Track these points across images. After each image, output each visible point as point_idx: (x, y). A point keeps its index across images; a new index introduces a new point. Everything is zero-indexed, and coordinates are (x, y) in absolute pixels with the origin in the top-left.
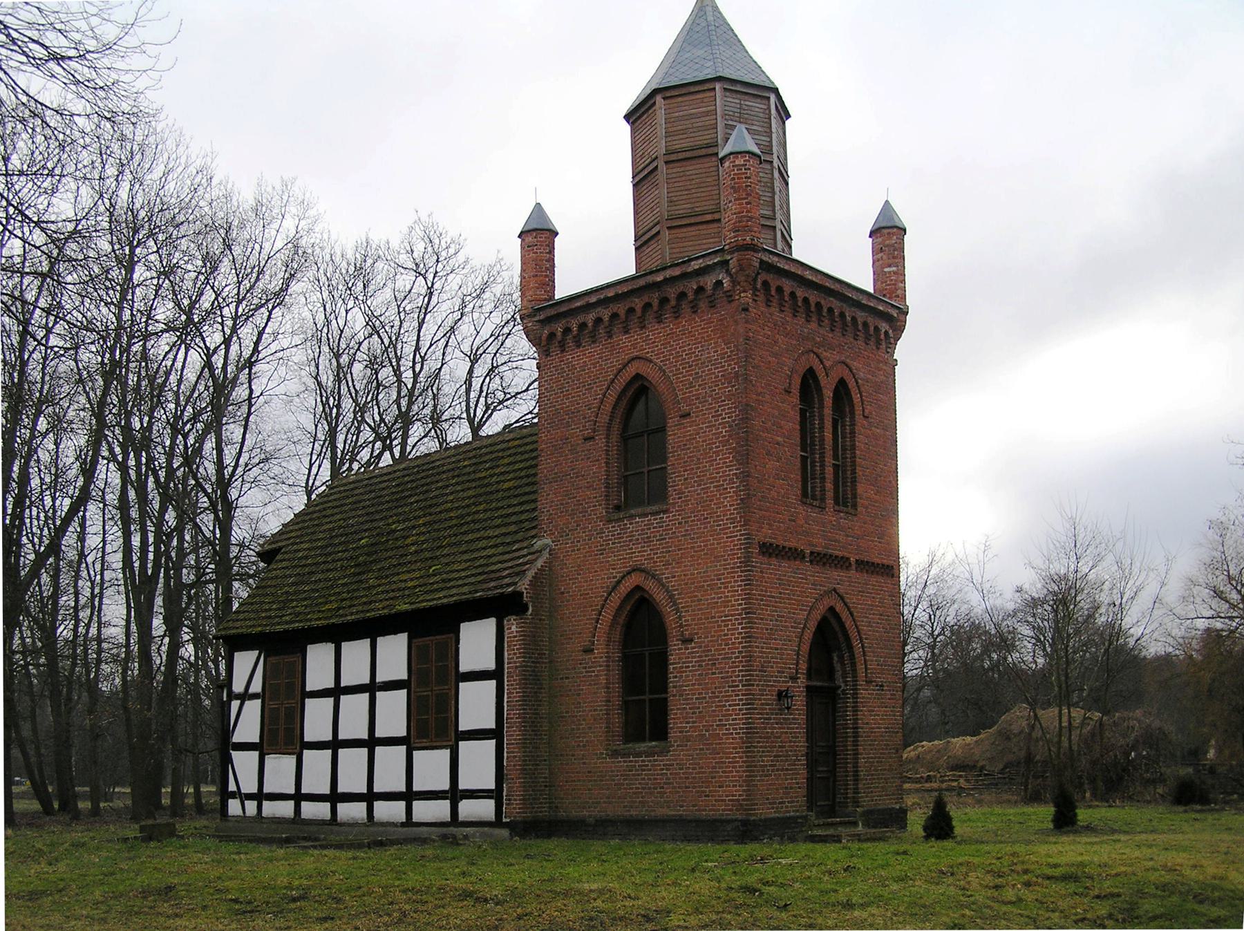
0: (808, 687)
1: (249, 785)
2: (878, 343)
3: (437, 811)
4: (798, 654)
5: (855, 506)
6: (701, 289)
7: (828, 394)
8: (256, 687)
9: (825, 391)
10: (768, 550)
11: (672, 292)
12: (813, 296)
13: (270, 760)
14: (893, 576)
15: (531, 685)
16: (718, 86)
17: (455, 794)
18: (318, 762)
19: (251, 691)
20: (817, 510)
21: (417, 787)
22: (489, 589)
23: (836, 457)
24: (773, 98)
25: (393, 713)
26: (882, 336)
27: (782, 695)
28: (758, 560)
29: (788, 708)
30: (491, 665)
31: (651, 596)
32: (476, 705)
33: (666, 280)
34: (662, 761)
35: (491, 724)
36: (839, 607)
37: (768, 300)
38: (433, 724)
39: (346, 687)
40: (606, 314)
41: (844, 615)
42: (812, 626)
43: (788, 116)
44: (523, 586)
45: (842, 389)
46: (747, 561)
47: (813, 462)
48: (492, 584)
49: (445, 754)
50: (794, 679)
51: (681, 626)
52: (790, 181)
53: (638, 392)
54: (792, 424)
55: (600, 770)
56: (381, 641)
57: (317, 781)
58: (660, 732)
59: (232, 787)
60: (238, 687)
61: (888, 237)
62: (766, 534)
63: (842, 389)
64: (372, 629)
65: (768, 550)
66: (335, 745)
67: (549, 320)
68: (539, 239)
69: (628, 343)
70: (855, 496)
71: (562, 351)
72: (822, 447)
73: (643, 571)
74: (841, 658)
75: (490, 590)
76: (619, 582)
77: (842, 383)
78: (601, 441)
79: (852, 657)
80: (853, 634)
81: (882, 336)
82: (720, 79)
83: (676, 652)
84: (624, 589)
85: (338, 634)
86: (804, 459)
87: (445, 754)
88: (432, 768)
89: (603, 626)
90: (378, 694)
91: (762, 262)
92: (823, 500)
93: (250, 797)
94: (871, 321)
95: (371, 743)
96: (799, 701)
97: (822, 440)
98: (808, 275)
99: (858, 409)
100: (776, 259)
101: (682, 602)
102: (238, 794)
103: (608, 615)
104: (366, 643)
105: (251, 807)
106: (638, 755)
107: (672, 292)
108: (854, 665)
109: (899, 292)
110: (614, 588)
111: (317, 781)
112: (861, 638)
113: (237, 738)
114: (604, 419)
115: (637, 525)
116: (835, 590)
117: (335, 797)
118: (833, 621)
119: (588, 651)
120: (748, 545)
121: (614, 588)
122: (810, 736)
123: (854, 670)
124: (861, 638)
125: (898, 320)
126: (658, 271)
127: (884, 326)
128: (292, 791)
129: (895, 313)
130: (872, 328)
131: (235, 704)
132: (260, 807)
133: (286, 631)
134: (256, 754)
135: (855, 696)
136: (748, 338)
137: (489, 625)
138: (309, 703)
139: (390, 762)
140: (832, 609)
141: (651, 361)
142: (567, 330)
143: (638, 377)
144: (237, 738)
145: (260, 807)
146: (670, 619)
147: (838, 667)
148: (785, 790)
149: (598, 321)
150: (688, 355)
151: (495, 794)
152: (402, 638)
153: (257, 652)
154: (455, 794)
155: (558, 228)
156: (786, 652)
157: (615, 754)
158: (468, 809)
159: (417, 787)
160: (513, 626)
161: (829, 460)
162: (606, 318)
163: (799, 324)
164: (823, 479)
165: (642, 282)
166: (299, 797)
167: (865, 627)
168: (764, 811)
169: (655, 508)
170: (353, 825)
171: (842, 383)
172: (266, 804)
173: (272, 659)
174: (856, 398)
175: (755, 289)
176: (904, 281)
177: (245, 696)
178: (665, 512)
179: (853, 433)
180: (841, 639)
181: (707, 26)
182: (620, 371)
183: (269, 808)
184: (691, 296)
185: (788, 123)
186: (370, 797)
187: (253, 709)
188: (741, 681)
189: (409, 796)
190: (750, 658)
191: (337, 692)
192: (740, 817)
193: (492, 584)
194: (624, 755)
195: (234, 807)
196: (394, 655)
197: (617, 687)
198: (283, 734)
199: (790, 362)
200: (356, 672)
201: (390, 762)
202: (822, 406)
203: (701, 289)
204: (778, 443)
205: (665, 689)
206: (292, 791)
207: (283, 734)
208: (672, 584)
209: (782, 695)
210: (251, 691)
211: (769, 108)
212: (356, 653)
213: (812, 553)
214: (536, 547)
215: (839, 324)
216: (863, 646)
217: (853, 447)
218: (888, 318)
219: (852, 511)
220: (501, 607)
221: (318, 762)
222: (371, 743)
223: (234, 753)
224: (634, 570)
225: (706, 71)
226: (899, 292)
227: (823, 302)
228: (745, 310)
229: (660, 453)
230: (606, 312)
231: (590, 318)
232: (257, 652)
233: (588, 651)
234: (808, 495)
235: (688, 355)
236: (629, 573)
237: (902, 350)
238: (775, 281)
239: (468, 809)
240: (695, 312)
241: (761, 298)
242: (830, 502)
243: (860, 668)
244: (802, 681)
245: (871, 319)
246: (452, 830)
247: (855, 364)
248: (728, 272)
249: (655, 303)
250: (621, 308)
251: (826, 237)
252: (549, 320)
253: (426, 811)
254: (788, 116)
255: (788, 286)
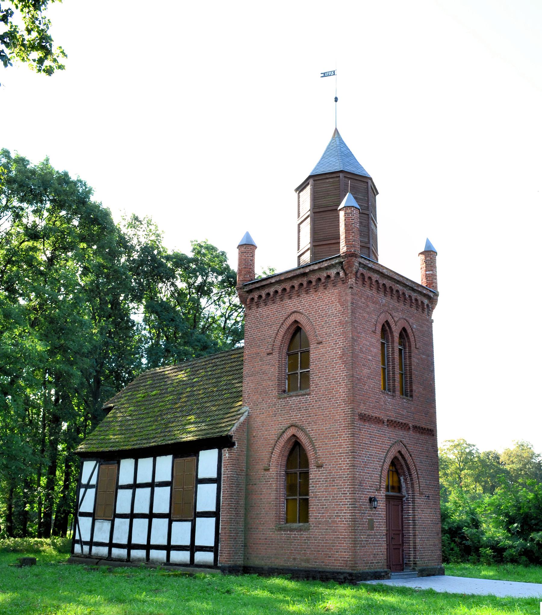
0: (386, 496)
1: (86, 537)
2: (423, 309)
3: (183, 557)
4: (381, 477)
5: (411, 396)
6: (328, 277)
7: (396, 335)
8: (93, 481)
9: (395, 334)
10: (364, 418)
11: (313, 278)
12: (388, 283)
13: (98, 524)
14: (433, 435)
15: (238, 490)
16: (341, 175)
17: (193, 548)
18: (122, 525)
19: (91, 483)
20: (391, 397)
21: (173, 543)
22: (215, 433)
23: (401, 369)
24: (369, 181)
25: (163, 500)
26: (425, 307)
27: (372, 500)
28: (358, 423)
29: (375, 508)
30: (214, 475)
31: (300, 440)
32: (206, 497)
33: (310, 271)
34: (305, 534)
35: (213, 509)
36: (404, 451)
37: (411, 305)
38: (183, 509)
39: (121, 486)
40: (279, 288)
41: (407, 456)
42: (388, 461)
43: (378, 193)
44: (232, 431)
45: (404, 334)
46: (353, 422)
47: (389, 371)
48: (217, 430)
49: (188, 525)
50: (378, 490)
51: (316, 458)
52: (378, 225)
53: (297, 330)
54: (376, 350)
55: (271, 539)
56: (158, 458)
57: (121, 537)
58: (304, 517)
59: (77, 537)
60: (84, 481)
61: (429, 255)
62: (362, 409)
63: (404, 334)
64: (154, 452)
65: (364, 418)
66: (132, 516)
67: (250, 291)
68: (247, 249)
69: (292, 304)
70: (411, 391)
71: (257, 307)
72: (394, 364)
73: (296, 426)
74: (405, 480)
75: (215, 433)
76: (284, 432)
77: (404, 329)
78: (276, 355)
79: (412, 480)
80: (412, 467)
81: (425, 307)
82: (341, 171)
83: (314, 473)
84: (287, 436)
85: (137, 454)
86: (384, 369)
87: (188, 525)
88: (181, 533)
89: (275, 456)
90: (155, 488)
91: (360, 263)
92: (394, 391)
93: (86, 543)
94: (419, 298)
95: (151, 516)
96: (381, 504)
97: (393, 359)
98: (405, 282)
99: (413, 344)
100: (367, 262)
101: (317, 444)
102: (80, 542)
103: (277, 450)
104: (151, 460)
105: (86, 548)
106: (291, 530)
107: (313, 278)
108: (412, 484)
109: (434, 284)
110: (281, 435)
111: (121, 537)
112: (416, 470)
113: (82, 509)
114: (278, 343)
115: (294, 400)
116: (401, 441)
117: (130, 546)
118: (400, 458)
119: (267, 470)
120: (353, 414)
121: (281, 435)
122: (388, 524)
123: (413, 487)
124: (416, 470)
125: (433, 299)
126: (307, 266)
127: (426, 301)
128: (107, 541)
129: (432, 295)
130: (420, 302)
131: (82, 490)
132: (90, 549)
133: (110, 452)
134: (90, 519)
135: (413, 502)
136: (352, 303)
137: (214, 453)
138: (120, 492)
139: (160, 526)
140: (399, 452)
141: (302, 314)
142: (260, 297)
143: (296, 322)
144: (82, 509)
145: (90, 549)
146: (311, 455)
147: (404, 485)
148: (376, 551)
149: (276, 292)
150: (325, 313)
151: (214, 549)
152: (170, 458)
153: (95, 462)
154: (193, 548)
155: (257, 245)
156: (375, 476)
157: (280, 529)
158: (200, 557)
159: (173, 543)
160: (226, 453)
161: (397, 371)
162: (280, 291)
163: (384, 300)
164: (394, 381)
165: (298, 272)
166: (111, 545)
167: (417, 462)
168: (362, 568)
169: (303, 392)
170: (139, 560)
171: (404, 329)
172: (94, 548)
173: (103, 467)
174: (412, 339)
175: (356, 277)
176: (436, 279)
177: (88, 486)
178: (308, 394)
179: (410, 356)
180: (405, 469)
181: (338, 147)
182: (286, 318)
183: (95, 550)
184: (323, 280)
185: (377, 197)
186: (148, 547)
187: (91, 492)
188: (348, 491)
189: (169, 548)
190: (354, 478)
191: (134, 486)
192: (348, 571)
193: (217, 430)
194: (285, 530)
195: (77, 548)
196: (165, 466)
197: (283, 491)
198: (105, 510)
199: (375, 317)
200: (144, 477)
201: (160, 526)
202: (393, 342)
203: (328, 277)
204: (369, 360)
205: (307, 494)
206: (107, 541)
207: (105, 510)
208: (312, 434)
209: (372, 500)
210: (91, 483)
211: (367, 188)
212: (145, 464)
213: (388, 420)
214: (241, 411)
215: (402, 299)
216: (417, 474)
217: (410, 364)
218: (429, 297)
219: (411, 399)
220: (221, 442)
221: (122, 525)
222: (151, 516)
223: (79, 518)
224: (292, 426)
225: (336, 168)
226: (434, 284)
227: (393, 287)
228: (351, 288)
229: (306, 363)
230: (280, 287)
231: (272, 290)
232: (95, 462)
233: (267, 470)
234: (388, 388)
235: (325, 313)
236: (289, 427)
237: (437, 315)
238: (367, 274)
239: (200, 557)
240: (325, 289)
241: (360, 282)
242: (398, 393)
243: (416, 486)
244: (383, 493)
245: (420, 298)
246: (190, 569)
247: (411, 321)
248: (342, 268)
249: (305, 284)
250: (288, 286)
251: (398, 255)
252: (250, 291)
253: (178, 556)
254: (378, 193)
255: (375, 277)
